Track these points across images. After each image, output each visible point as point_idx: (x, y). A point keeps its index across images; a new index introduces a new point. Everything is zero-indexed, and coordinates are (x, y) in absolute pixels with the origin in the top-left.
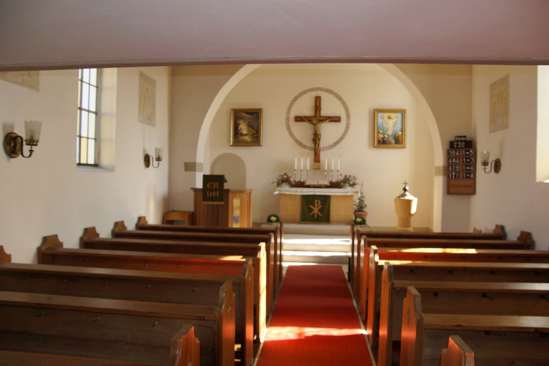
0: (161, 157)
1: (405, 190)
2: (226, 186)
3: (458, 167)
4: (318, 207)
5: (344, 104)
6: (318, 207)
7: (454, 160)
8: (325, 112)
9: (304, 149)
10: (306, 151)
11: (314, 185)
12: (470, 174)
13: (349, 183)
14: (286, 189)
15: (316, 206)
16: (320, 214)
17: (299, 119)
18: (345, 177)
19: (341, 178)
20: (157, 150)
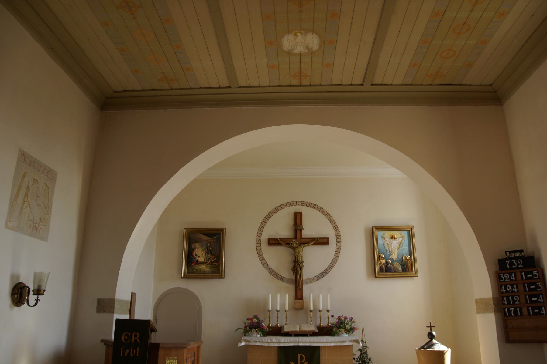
0: (43, 288)
1: (431, 336)
2: (154, 338)
3: (517, 298)
5: (332, 222)
7: (510, 288)
8: (308, 232)
9: (280, 282)
10: (284, 284)
11: (296, 331)
12: (540, 308)
13: (344, 328)
14: (257, 339)
17: (273, 242)
18: (339, 318)
19: (333, 321)
20: (38, 277)
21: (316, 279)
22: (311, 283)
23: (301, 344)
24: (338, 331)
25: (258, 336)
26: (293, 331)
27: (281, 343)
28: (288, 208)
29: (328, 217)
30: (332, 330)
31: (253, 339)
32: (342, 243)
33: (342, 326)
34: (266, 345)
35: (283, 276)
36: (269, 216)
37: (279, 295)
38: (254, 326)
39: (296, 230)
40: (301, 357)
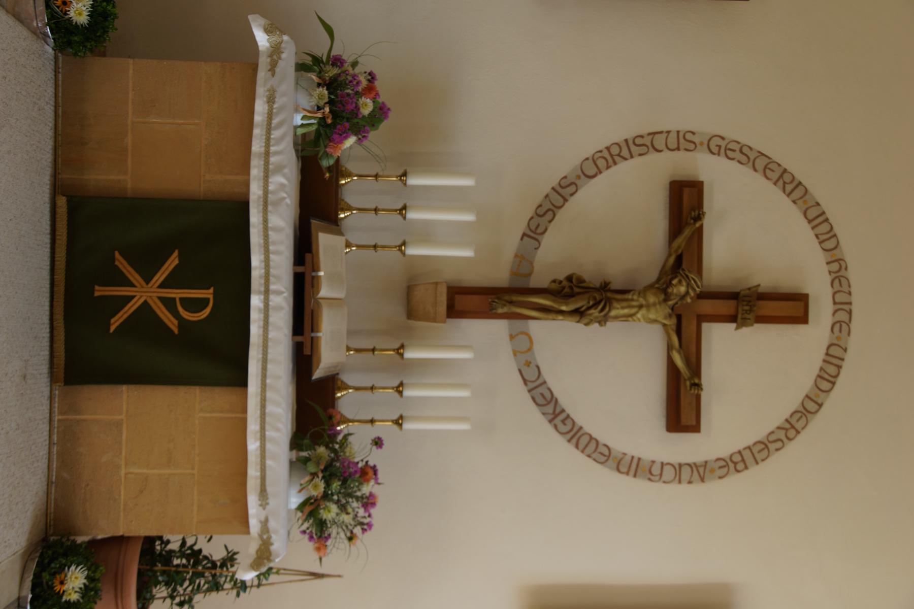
4: (169, 303)
6: (169, 303)
8: (721, 342)
9: (521, 227)
10: (511, 242)
11: (315, 282)
14: (283, 112)
15: (177, 294)
16: (116, 322)
17: (685, 204)
18: (368, 472)
19: (359, 449)
21: (531, 374)
22: (515, 353)
23: (256, 301)
24: (311, 468)
25: (298, 120)
26: (315, 268)
27: (266, 177)
28: (825, 268)
29: (781, 435)
30: (317, 439)
31: (283, 88)
32: (674, 488)
33: (336, 485)
34: (257, 146)
35: (546, 240)
36: (789, 184)
37: (469, 217)
38: (344, 101)
39: (734, 296)
40: (203, 303)
